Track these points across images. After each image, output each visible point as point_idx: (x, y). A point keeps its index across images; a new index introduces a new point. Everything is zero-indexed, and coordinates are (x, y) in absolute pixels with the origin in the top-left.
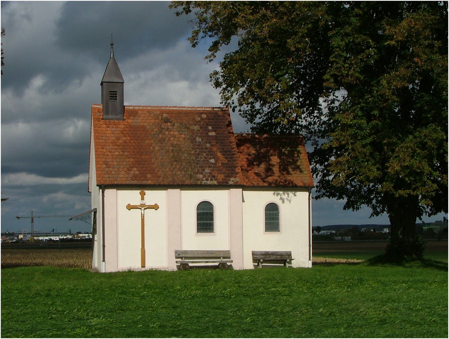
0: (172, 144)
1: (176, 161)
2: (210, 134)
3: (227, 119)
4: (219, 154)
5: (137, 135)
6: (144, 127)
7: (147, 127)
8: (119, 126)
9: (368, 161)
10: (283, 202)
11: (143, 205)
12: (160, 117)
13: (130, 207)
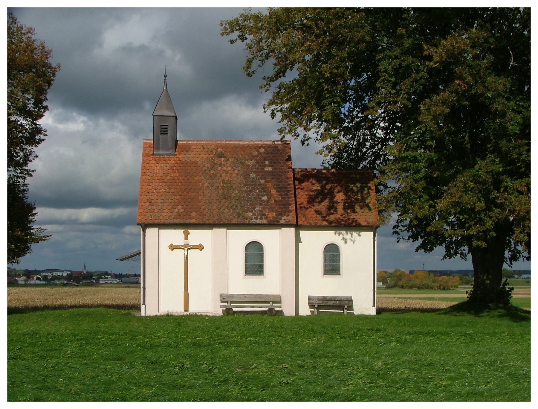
0: (223, 180)
1: (225, 198)
2: (266, 169)
3: (287, 153)
4: (273, 191)
7: (199, 163)
8: (169, 162)
9: (420, 197)
10: (346, 242)
11: (186, 245)
12: (214, 151)
13: (173, 247)
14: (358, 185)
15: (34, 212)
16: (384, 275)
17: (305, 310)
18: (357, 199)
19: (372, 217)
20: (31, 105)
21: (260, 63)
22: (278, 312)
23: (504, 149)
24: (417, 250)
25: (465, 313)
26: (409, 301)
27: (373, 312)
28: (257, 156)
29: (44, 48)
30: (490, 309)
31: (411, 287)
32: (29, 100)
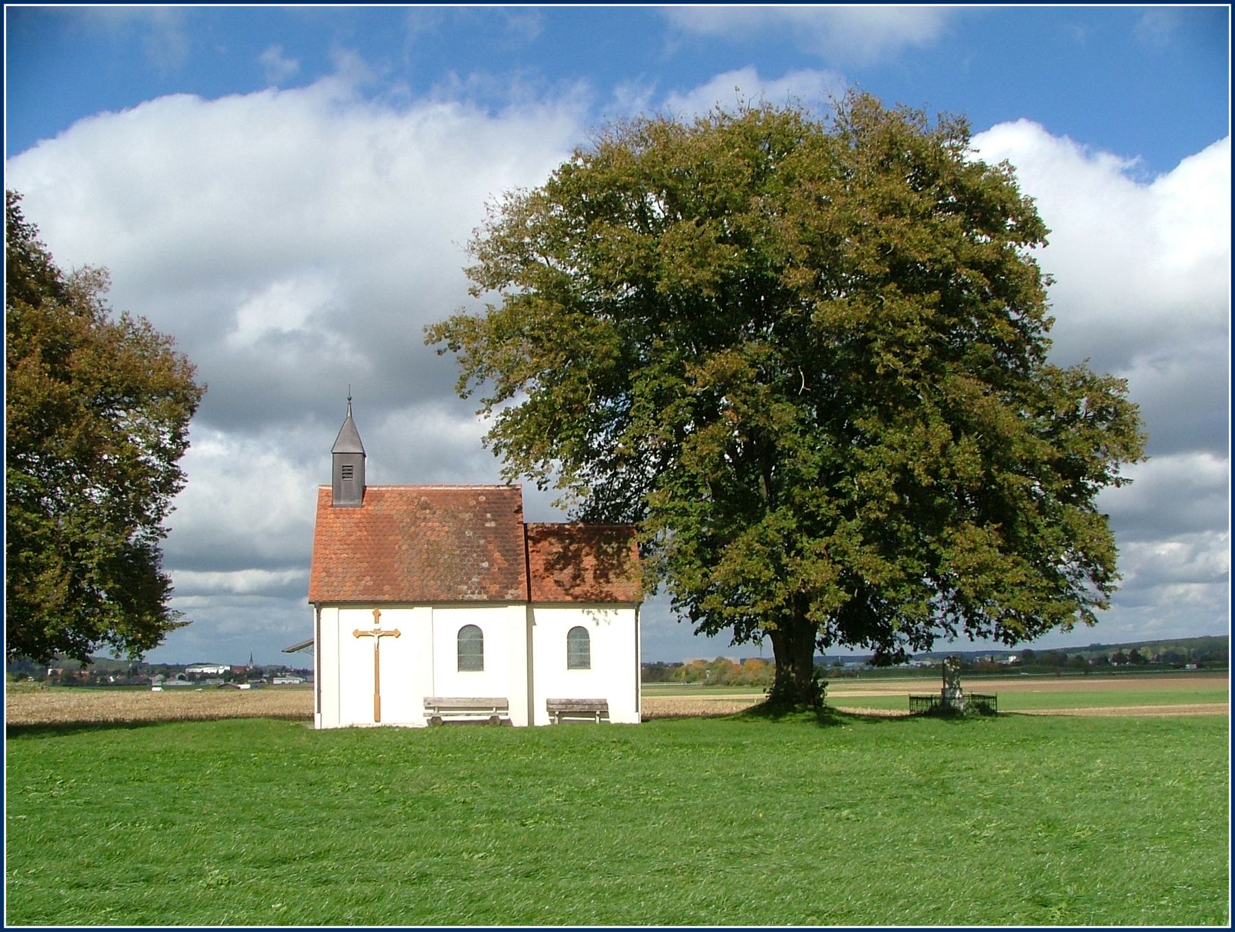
2: (487, 525)
4: (497, 555)
5: (378, 527)
6: (390, 517)
9: (690, 563)
13: (359, 634)
14: (615, 545)
15: (169, 586)
16: (701, 666)
17: (542, 719)
18: (612, 565)
19: (634, 589)
20: (166, 440)
21: (478, 380)
22: (502, 721)
23: (797, 499)
24: (696, 634)
25: (760, 719)
26: (726, 703)
27: (635, 719)
28: (475, 507)
29: (185, 362)
30: (795, 711)
31: (740, 684)
32: (164, 433)
